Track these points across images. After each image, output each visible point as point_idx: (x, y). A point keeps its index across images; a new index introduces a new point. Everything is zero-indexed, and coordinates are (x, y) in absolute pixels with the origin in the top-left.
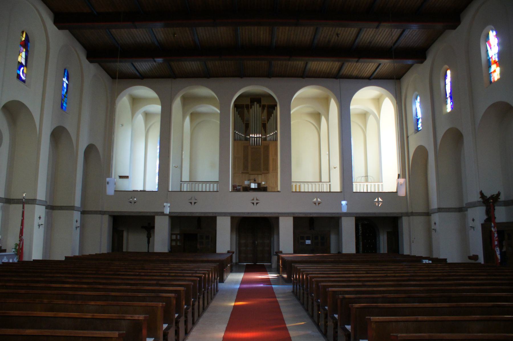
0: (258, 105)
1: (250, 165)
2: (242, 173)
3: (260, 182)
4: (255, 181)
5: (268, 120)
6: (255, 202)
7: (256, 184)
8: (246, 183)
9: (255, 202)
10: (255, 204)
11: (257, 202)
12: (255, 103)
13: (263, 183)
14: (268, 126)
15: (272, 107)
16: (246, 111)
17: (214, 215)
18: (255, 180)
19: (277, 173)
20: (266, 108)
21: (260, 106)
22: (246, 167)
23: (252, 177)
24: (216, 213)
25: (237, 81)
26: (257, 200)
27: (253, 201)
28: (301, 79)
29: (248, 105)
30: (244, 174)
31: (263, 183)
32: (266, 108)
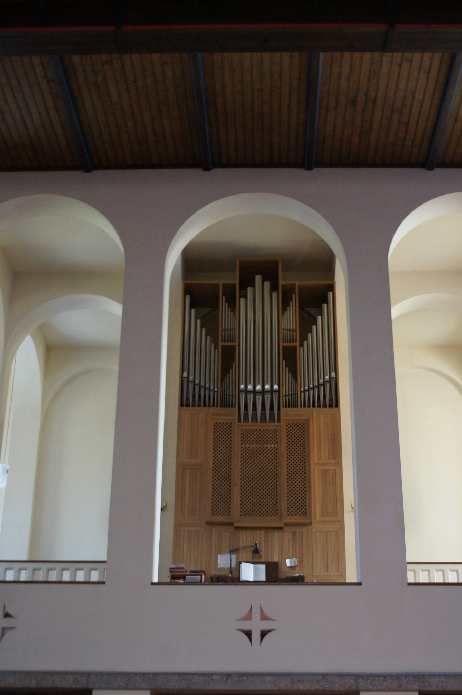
0: (267, 284)
1: (236, 492)
2: (208, 523)
3: (276, 559)
4: (255, 556)
5: (304, 337)
6: (256, 627)
7: (263, 567)
8: (224, 561)
9: (256, 627)
10: (256, 636)
11: (266, 625)
12: (258, 279)
13: (288, 562)
14: (303, 354)
15: (317, 299)
16: (223, 305)
17: (82, 684)
18: (256, 551)
19: (340, 534)
20: (295, 298)
21: (274, 287)
22: (221, 501)
23: (245, 539)
24: (88, 674)
25: (187, 181)
26: (264, 617)
27: (246, 626)
28: (422, 172)
29: (233, 287)
30: (214, 529)
31: (288, 562)
32: (295, 298)
